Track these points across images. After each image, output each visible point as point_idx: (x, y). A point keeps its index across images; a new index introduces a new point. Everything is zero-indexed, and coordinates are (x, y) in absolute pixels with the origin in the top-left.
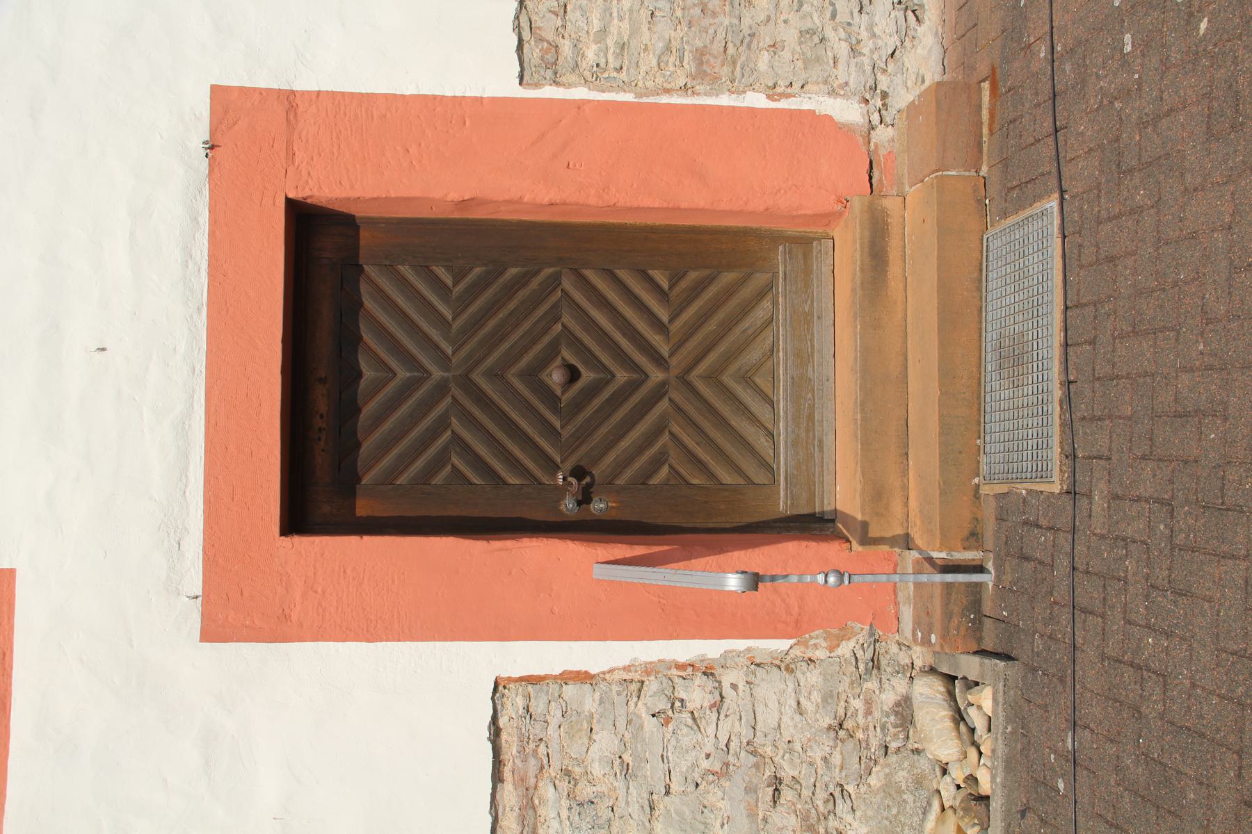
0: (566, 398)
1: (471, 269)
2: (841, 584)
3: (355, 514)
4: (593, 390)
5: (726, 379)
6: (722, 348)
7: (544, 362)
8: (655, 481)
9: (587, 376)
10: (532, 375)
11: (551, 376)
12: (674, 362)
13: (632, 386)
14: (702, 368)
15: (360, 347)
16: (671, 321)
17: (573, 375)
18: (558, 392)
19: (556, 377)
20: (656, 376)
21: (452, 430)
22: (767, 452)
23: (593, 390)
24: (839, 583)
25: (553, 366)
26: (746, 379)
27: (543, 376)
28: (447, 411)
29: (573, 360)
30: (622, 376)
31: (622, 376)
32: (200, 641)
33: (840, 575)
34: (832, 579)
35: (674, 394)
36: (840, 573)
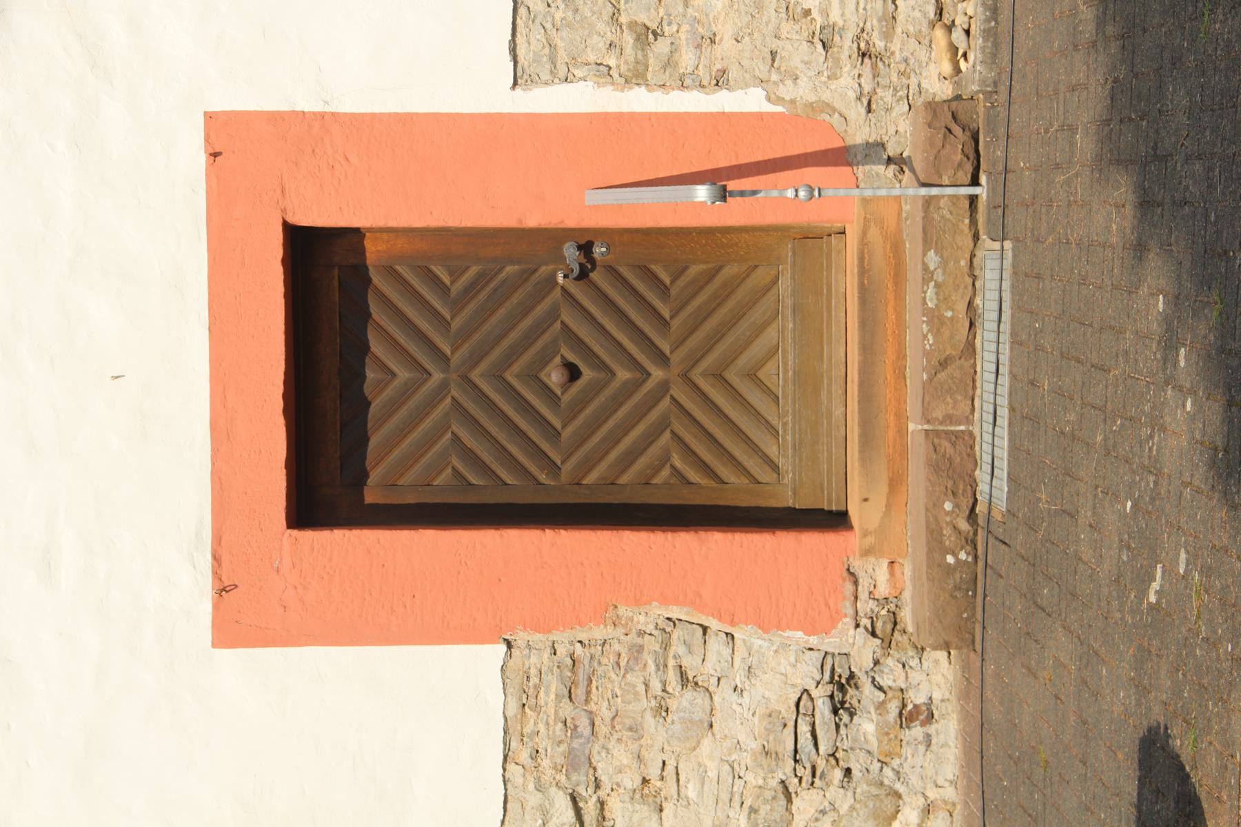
0: (566, 398)
1: (468, 268)
2: (811, 198)
3: (363, 499)
4: (596, 388)
5: (731, 375)
6: (729, 340)
7: (543, 360)
8: (657, 480)
9: (588, 374)
10: (533, 377)
11: (550, 375)
12: (675, 358)
13: (629, 389)
14: (705, 364)
15: (369, 325)
16: (672, 317)
17: (573, 373)
18: (558, 392)
19: (555, 377)
20: (657, 374)
21: (452, 432)
22: (772, 451)
23: (596, 388)
24: (809, 197)
25: (548, 382)
26: (752, 376)
27: (542, 376)
28: (447, 414)
29: (572, 358)
30: (623, 375)
31: (623, 375)
32: (214, 645)
33: (811, 189)
34: (802, 194)
35: (675, 392)
36: (810, 187)
